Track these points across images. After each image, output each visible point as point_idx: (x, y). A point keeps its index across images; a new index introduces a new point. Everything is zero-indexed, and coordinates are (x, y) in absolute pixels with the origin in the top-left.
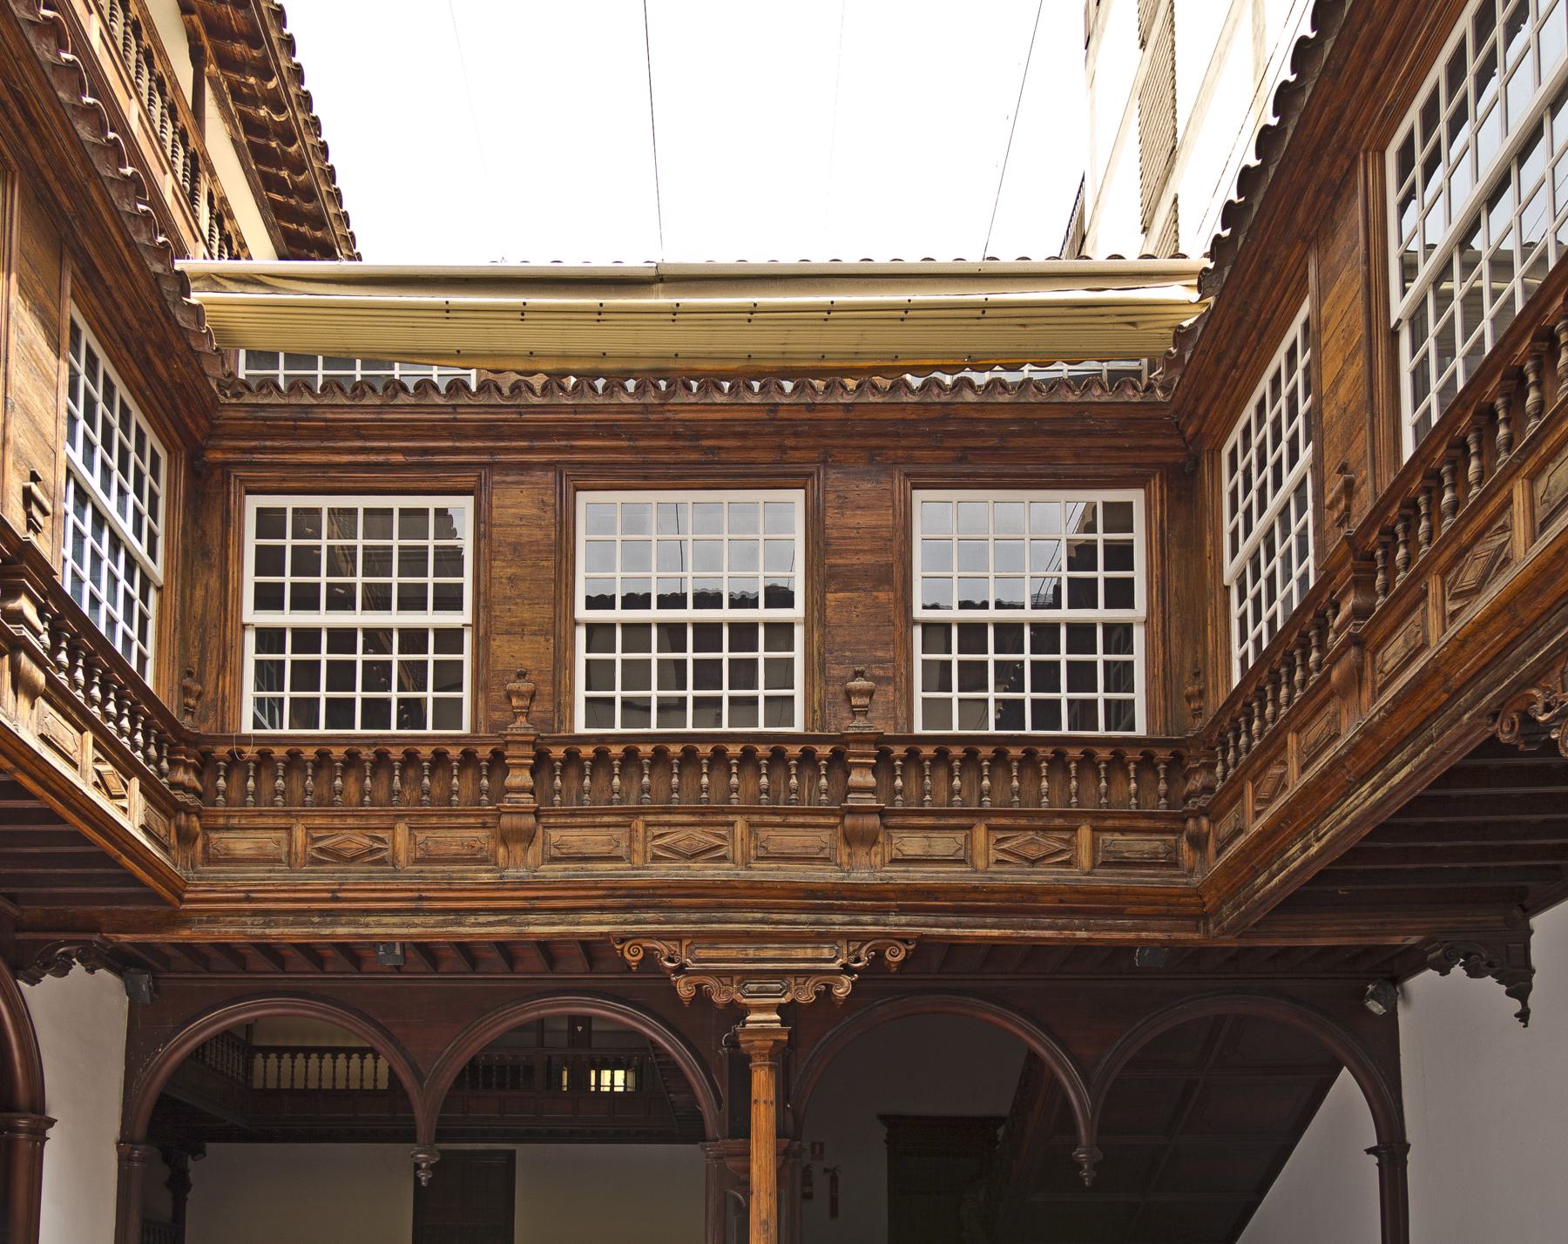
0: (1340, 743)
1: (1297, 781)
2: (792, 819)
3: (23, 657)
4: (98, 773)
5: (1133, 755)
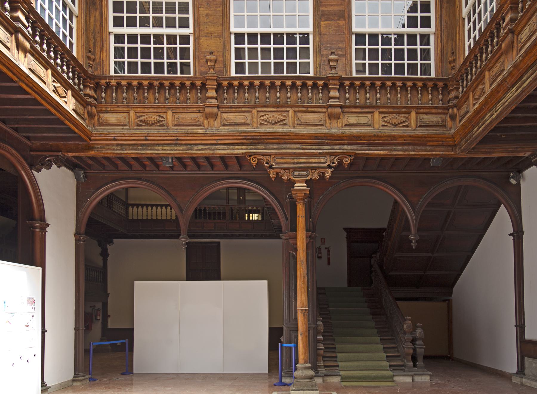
0: (504, 73)
1: (488, 89)
2: (310, 109)
3: (20, 36)
4: (54, 86)
5: (430, 84)
